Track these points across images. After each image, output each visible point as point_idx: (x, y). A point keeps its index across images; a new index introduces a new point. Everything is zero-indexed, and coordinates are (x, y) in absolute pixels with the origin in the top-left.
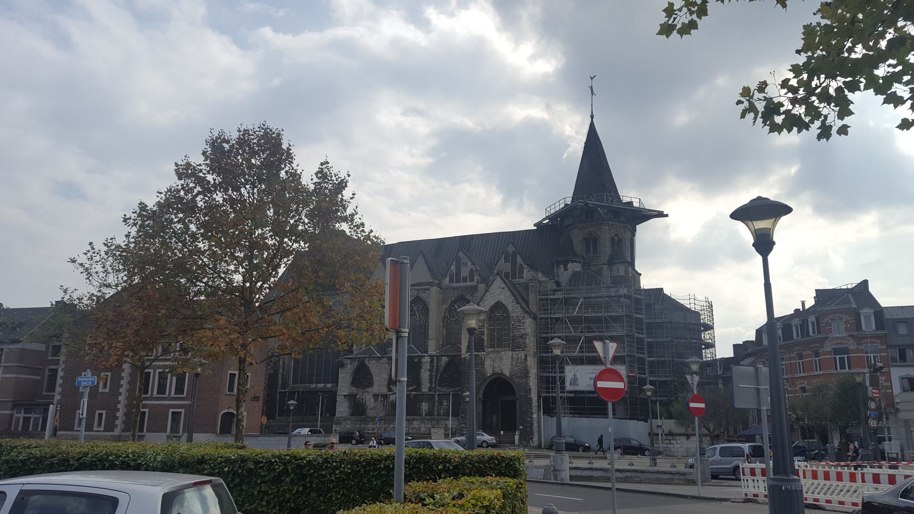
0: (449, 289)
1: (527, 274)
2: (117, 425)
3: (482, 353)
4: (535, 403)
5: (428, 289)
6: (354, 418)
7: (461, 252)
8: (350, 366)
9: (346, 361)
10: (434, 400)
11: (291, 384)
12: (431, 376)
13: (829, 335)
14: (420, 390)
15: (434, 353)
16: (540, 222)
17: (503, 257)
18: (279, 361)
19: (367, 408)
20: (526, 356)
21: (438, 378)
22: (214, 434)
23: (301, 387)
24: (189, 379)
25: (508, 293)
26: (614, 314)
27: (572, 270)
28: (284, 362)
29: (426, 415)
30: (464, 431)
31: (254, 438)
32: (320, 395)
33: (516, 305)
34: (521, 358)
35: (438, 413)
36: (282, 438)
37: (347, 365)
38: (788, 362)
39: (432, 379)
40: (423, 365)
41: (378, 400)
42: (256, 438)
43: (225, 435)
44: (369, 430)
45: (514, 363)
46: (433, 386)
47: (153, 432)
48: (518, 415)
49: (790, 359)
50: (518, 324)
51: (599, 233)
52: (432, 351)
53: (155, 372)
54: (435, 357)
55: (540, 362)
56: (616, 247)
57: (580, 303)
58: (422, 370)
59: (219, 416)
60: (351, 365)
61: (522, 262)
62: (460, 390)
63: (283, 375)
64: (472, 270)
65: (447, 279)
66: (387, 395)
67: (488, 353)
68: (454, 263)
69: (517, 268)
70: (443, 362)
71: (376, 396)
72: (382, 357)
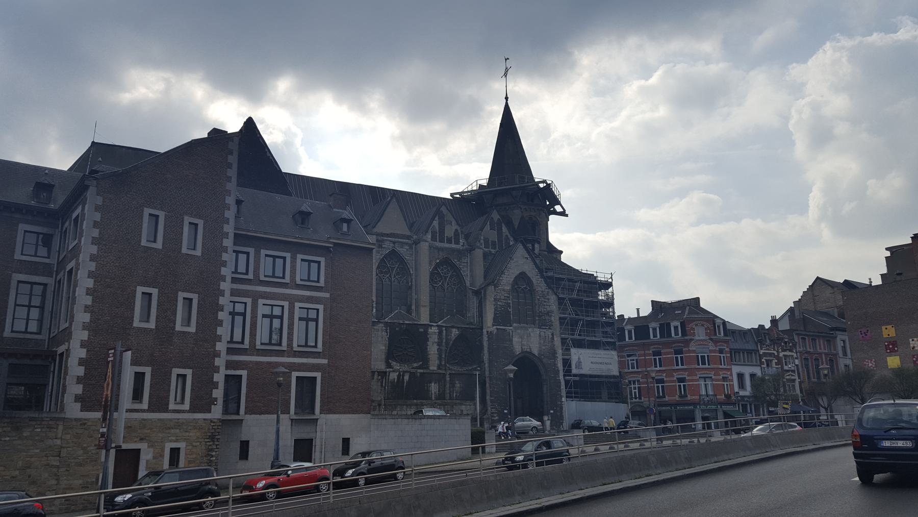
2: (216, 399)
12: (439, 350)
14: (427, 368)
17: (488, 223)
29: (436, 399)
30: (494, 417)
31: (417, 420)
33: (540, 279)
34: (548, 337)
35: (450, 396)
39: (442, 355)
46: (443, 363)
47: (261, 413)
49: (645, 355)
51: (539, 219)
54: (444, 329)
58: (429, 343)
61: (507, 233)
64: (456, 230)
70: (453, 335)
72: (379, 322)
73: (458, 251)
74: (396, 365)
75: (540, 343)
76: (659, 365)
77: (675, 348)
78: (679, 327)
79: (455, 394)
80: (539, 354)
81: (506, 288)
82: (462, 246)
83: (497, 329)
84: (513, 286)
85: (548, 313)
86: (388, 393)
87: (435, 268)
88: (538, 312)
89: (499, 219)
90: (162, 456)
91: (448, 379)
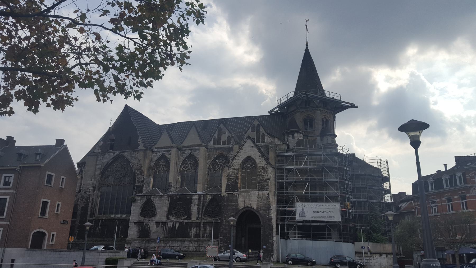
0: (212, 149)
1: (267, 140)
3: (237, 192)
4: (275, 229)
5: (199, 149)
6: (141, 239)
7: (222, 124)
8: (140, 201)
9: (136, 198)
10: (200, 226)
11: (97, 214)
12: (198, 209)
13: (473, 185)
14: (190, 219)
15: (202, 193)
16: (272, 110)
17: (251, 128)
18: (89, 197)
19: (151, 232)
20: (268, 194)
21: (204, 211)
22: (25, 249)
23: (104, 217)
24: (8, 204)
26: (330, 166)
27: (297, 138)
28: (93, 199)
29: (194, 237)
30: (222, 249)
31: (57, 252)
32: (117, 222)
33: (262, 159)
34: (265, 196)
35: (203, 236)
36: (80, 253)
37: (138, 201)
38: (439, 204)
40: (193, 201)
41: (159, 226)
42: (59, 252)
43: (34, 250)
44: (151, 248)
45: (260, 200)
46: (200, 216)
48: (262, 238)
49: (441, 202)
50: (263, 172)
51: (314, 116)
52: (200, 191)
54: (202, 196)
55: (277, 200)
56: (325, 125)
57: (306, 159)
58: (192, 205)
59: (31, 234)
60: (141, 201)
61: (264, 132)
62: (220, 219)
63: (91, 207)
64: (229, 136)
65: (212, 143)
66: (166, 222)
67: (241, 192)
68: (217, 132)
69: (261, 135)
70: (207, 199)
71: (158, 223)
72: (164, 195)
74: (172, 218)
76: (466, 208)
77: (461, 195)
78: (462, 177)
79: (206, 235)
81: (236, 167)
82: (232, 145)
83: (228, 194)
86: (166, 234)
88: (258, 180)
91: (202, 225)
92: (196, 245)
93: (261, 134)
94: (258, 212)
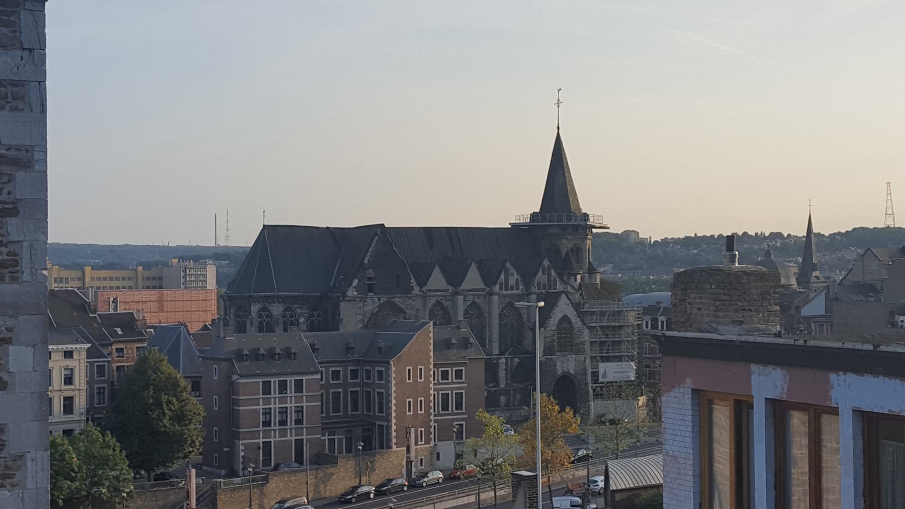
12: (506, 374)
14: (499, 387)
20: (585, 358)
25: (572, 309)
29: (505, 406)
46: (509, 382)
53: (452, 393)
61: (555, 276)
65: (498, 287)
68: (503, 273)
73: (518, 295)
75: (575, 365)
80: (574, 373)
83: (546, 358)
84: (558, 326)
85: (583, 343)
87: (502, 311)
89: (549, 265)
90: (418, 462)
91: (512, 392)
92: (508, 415)
93: (552, 278)
94: (575, 377)
